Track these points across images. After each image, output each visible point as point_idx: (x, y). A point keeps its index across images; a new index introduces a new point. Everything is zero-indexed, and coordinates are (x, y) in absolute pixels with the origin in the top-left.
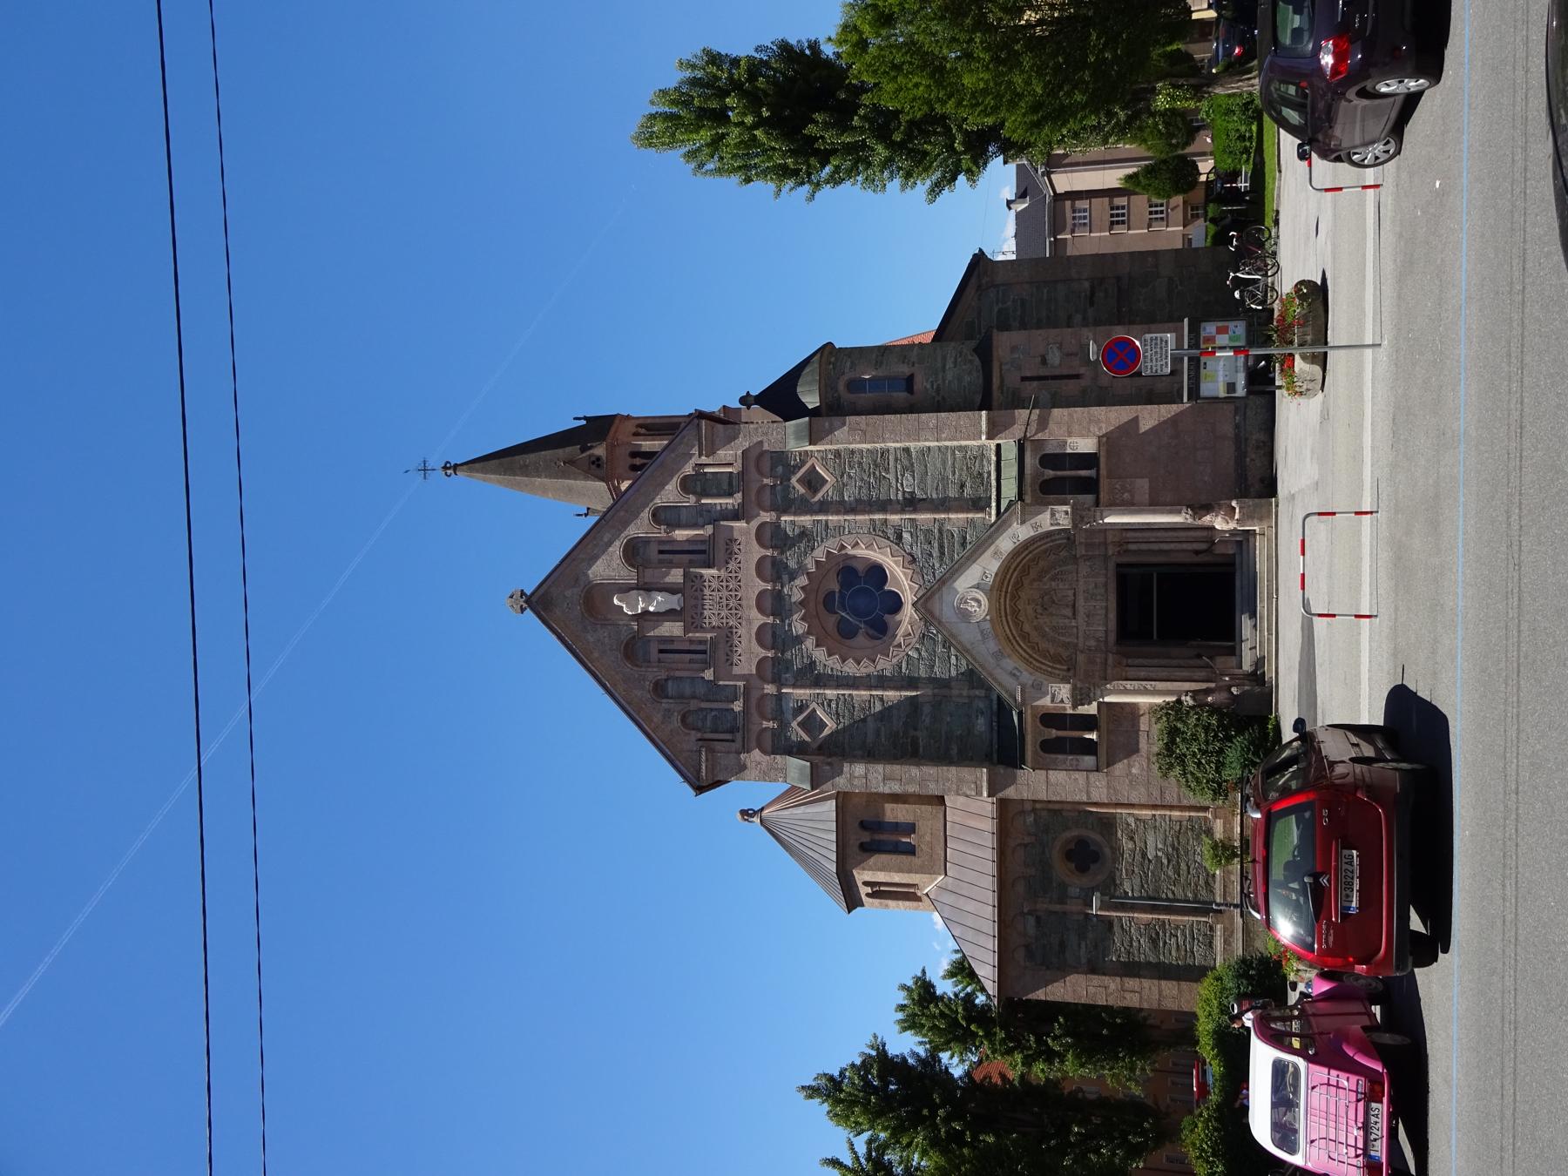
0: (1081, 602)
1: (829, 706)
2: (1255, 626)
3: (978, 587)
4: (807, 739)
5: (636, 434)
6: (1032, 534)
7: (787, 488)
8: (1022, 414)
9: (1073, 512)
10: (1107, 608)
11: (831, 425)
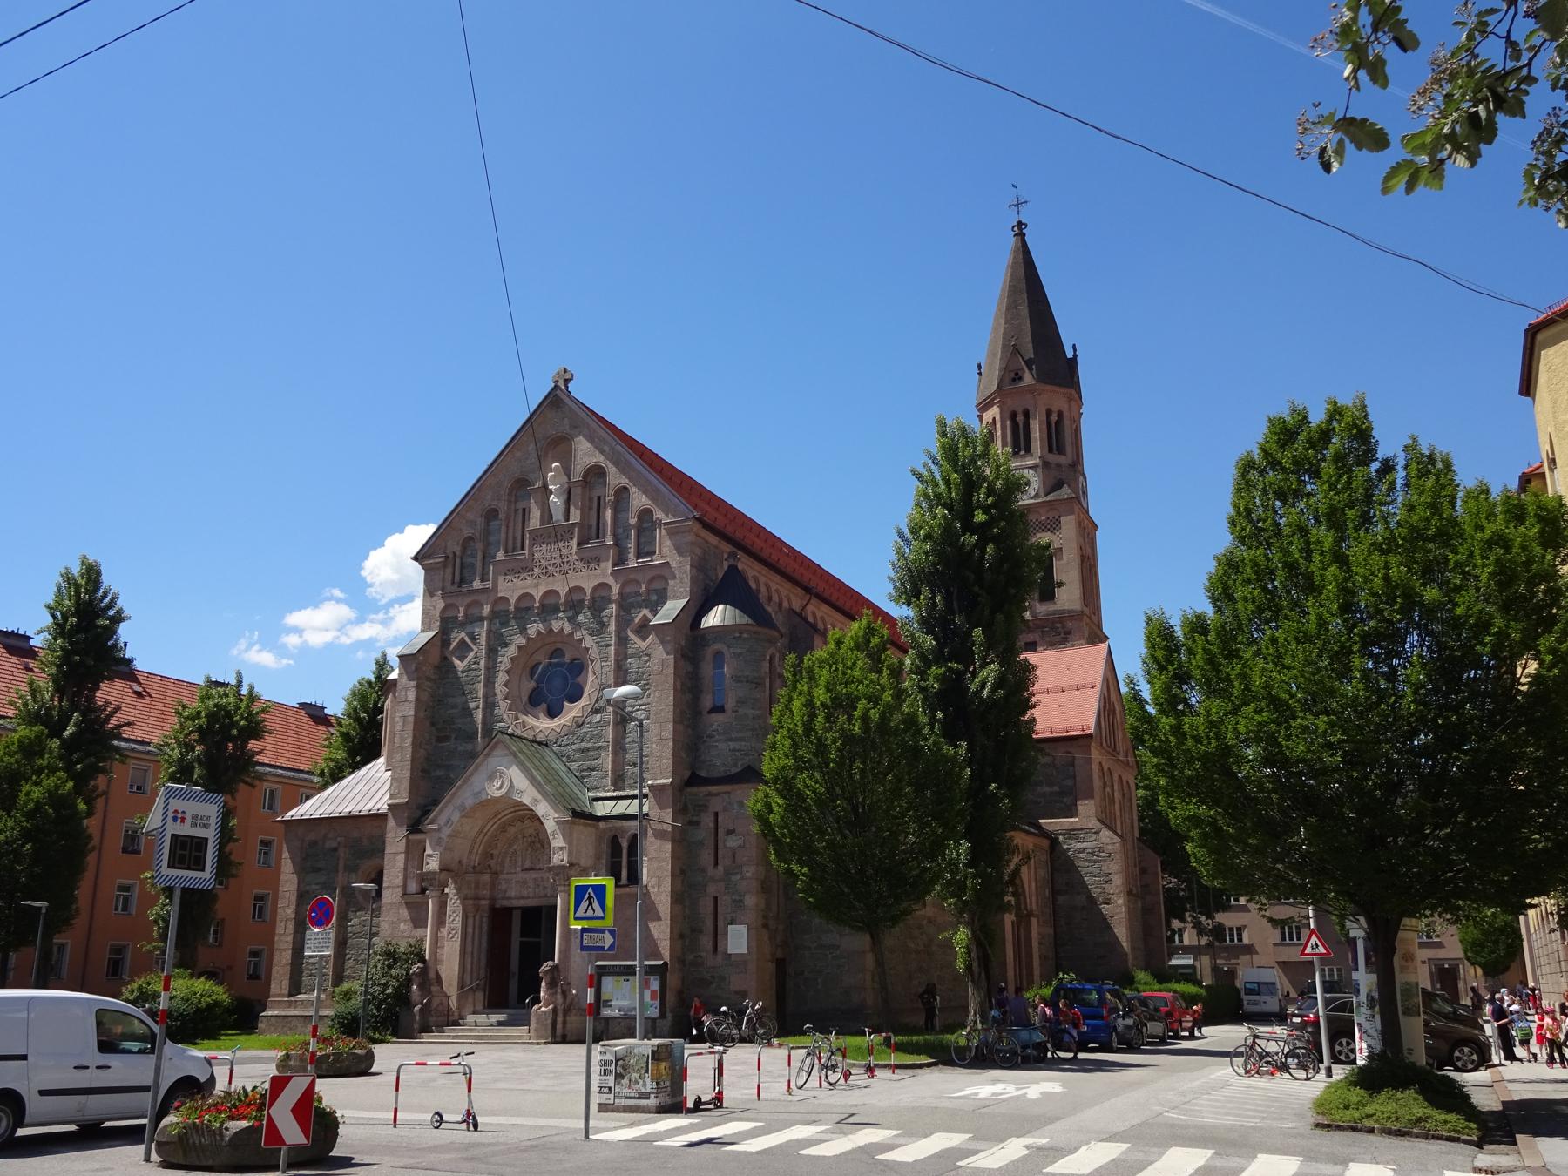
0: (534, 875)
1: (475, 663)
2: (492, 1025)
3: (511, 786)
4: (452, 647)
5: (1049, 413)
6: (549, 831)
7: (640, 606)
8: (667, 816)
9: (563, 866)
10: (528, 898)
11: (669, 642)
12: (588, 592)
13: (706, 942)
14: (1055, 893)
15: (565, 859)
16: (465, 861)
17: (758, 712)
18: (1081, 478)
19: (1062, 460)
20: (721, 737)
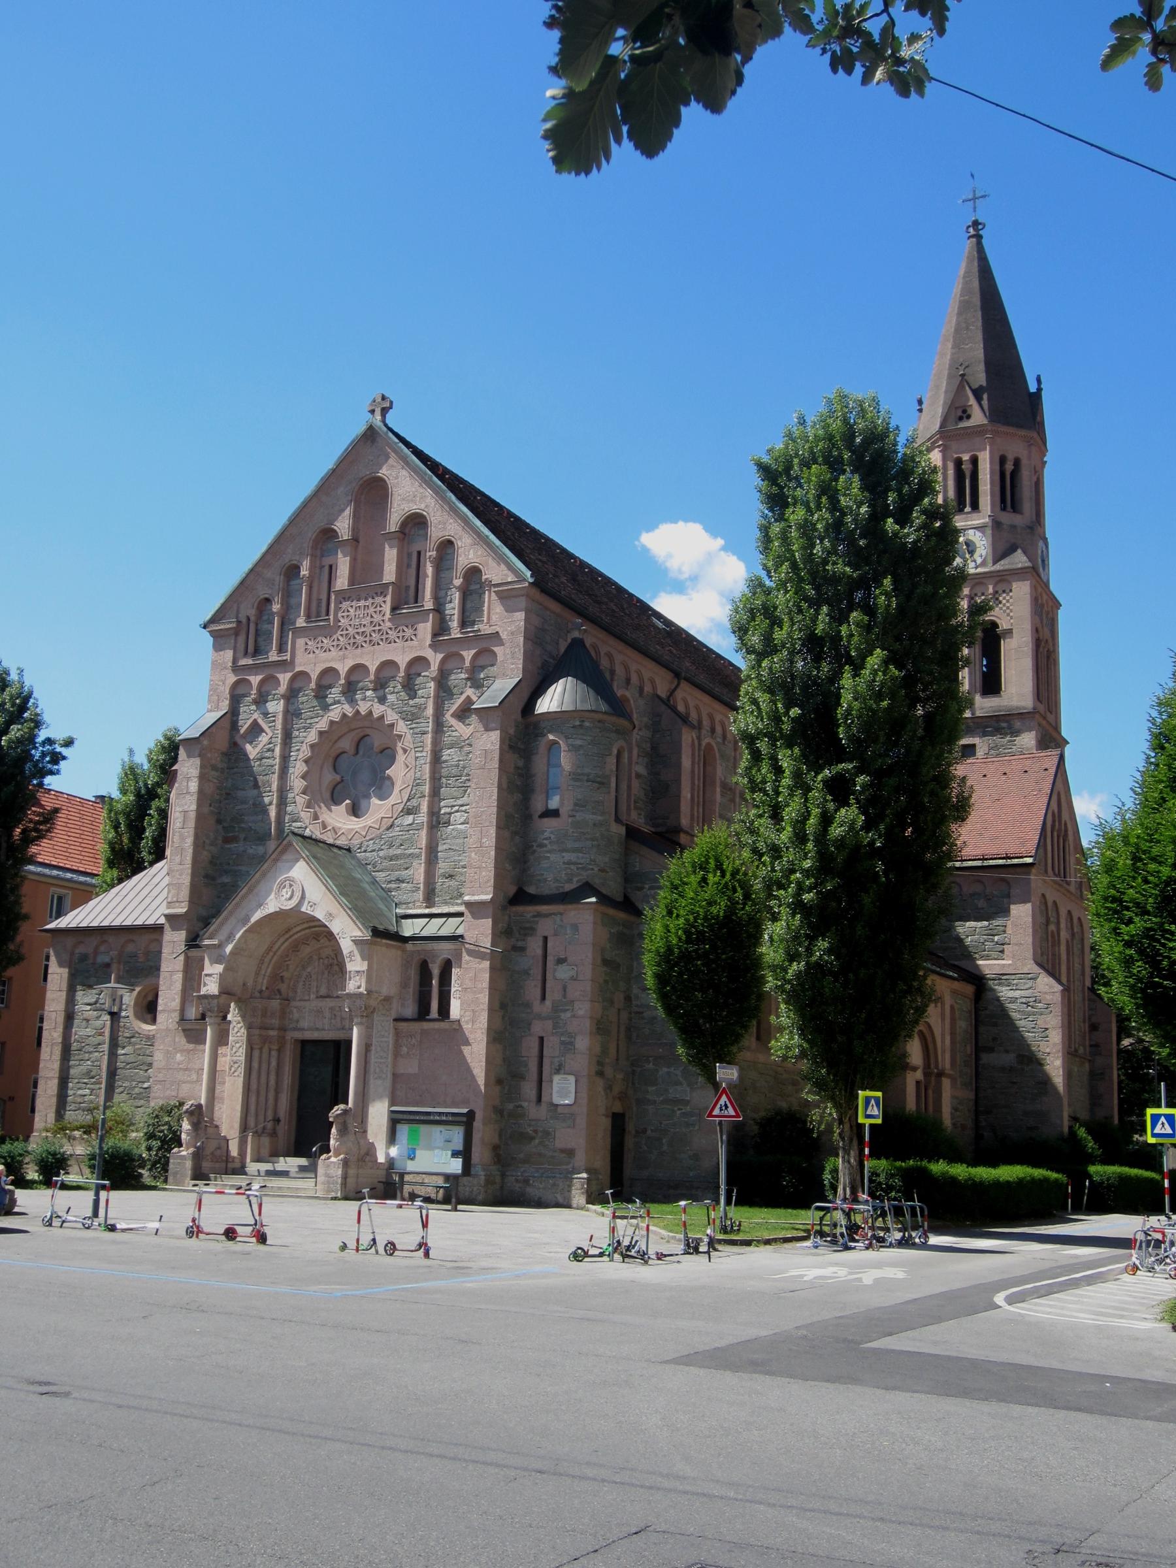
0: (330, 1003)
1: (269, 750)
9: (361, 994)
12: (403, 666)
13: (528, 1089)
14: (979, 1049)
15: (363, 985)
16: (250, 983)
17: (600, 818)
18: (1041, 544)
19: (1017, 520)
20: (555, 847)
